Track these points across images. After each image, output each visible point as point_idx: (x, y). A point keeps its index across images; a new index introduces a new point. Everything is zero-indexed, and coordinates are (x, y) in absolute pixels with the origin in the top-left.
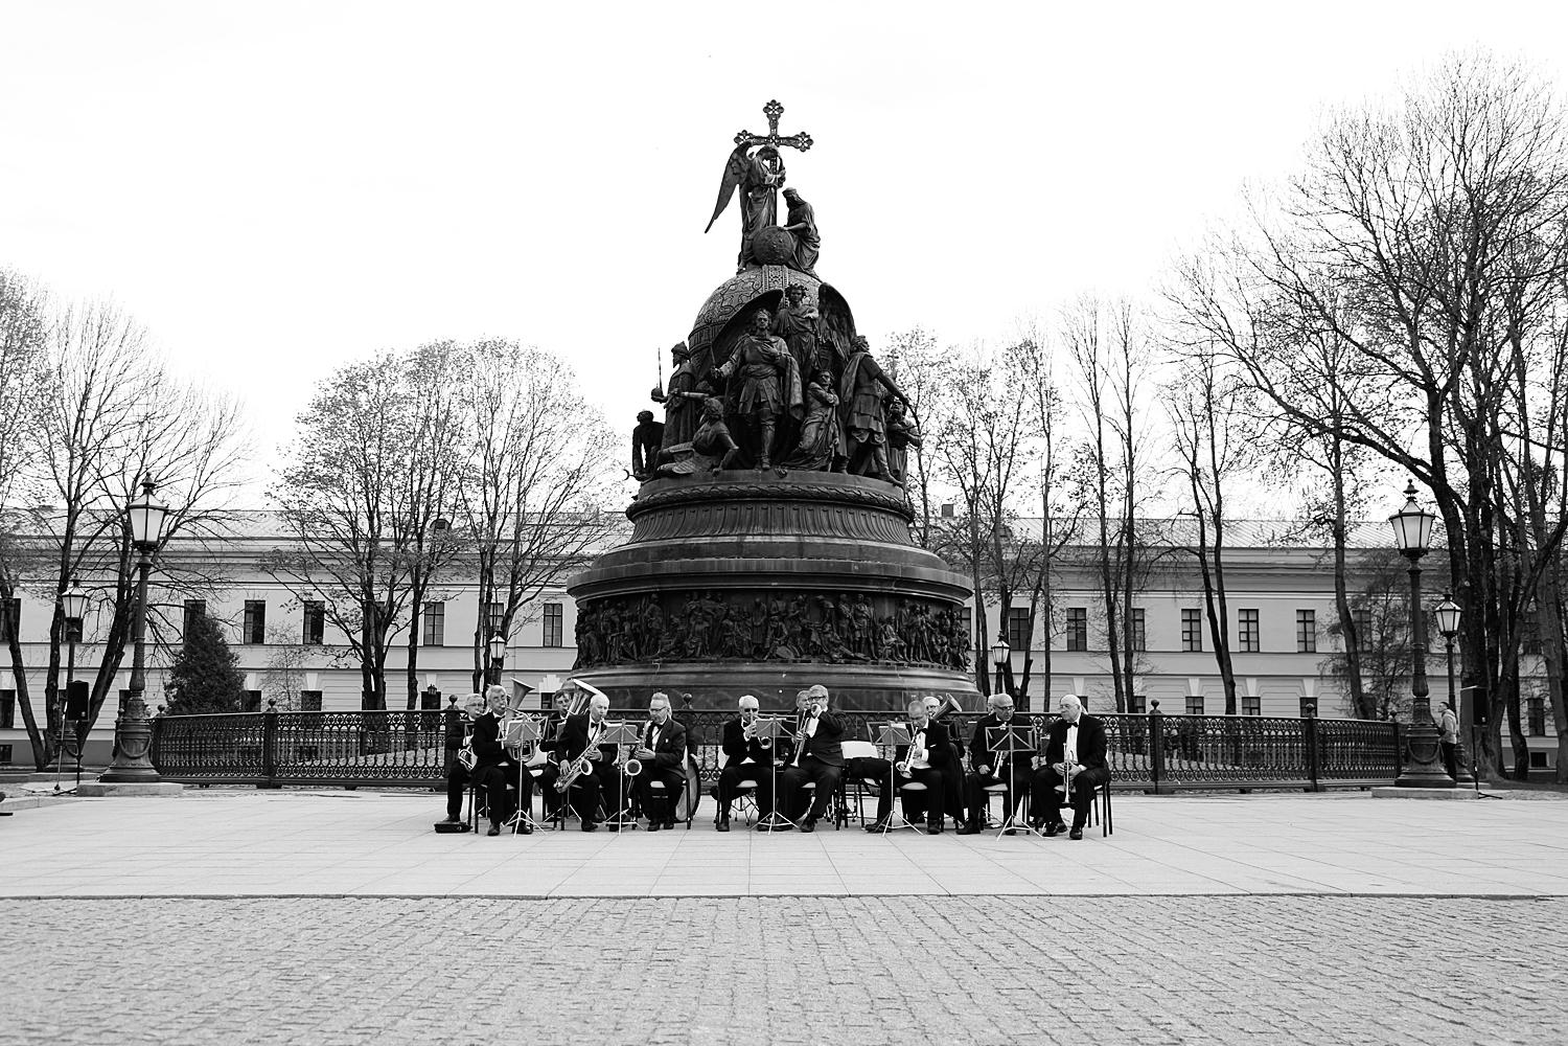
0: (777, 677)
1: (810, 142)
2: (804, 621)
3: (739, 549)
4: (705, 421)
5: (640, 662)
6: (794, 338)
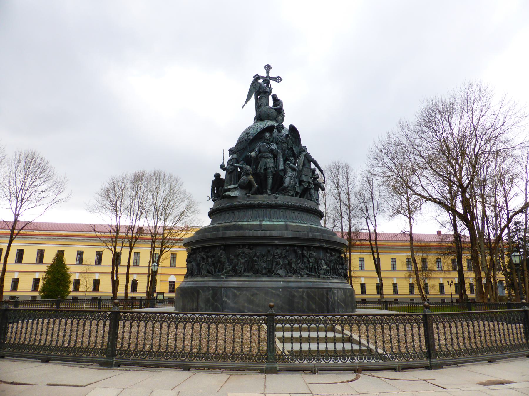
0: (279, 283)
1: (281, 79)
2: (289, 258)
3: (260, 227)
4: (243, 175)
5: (215, 276)
6: (279, 145)
